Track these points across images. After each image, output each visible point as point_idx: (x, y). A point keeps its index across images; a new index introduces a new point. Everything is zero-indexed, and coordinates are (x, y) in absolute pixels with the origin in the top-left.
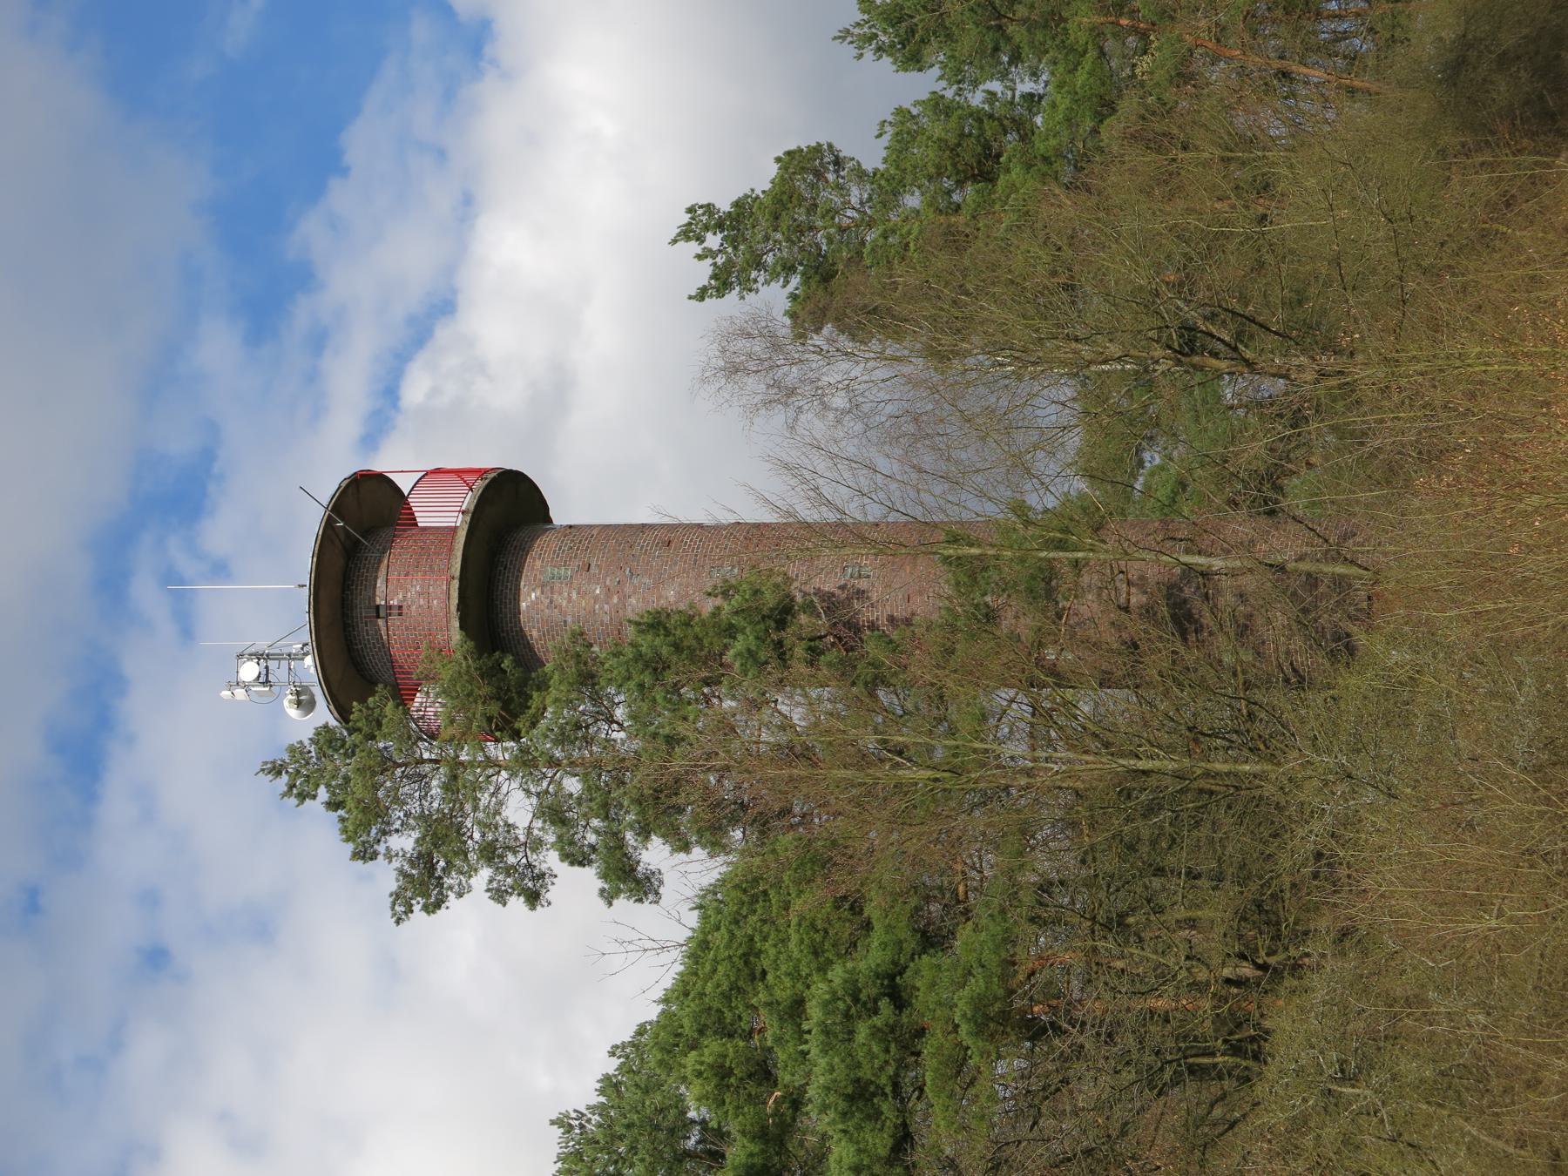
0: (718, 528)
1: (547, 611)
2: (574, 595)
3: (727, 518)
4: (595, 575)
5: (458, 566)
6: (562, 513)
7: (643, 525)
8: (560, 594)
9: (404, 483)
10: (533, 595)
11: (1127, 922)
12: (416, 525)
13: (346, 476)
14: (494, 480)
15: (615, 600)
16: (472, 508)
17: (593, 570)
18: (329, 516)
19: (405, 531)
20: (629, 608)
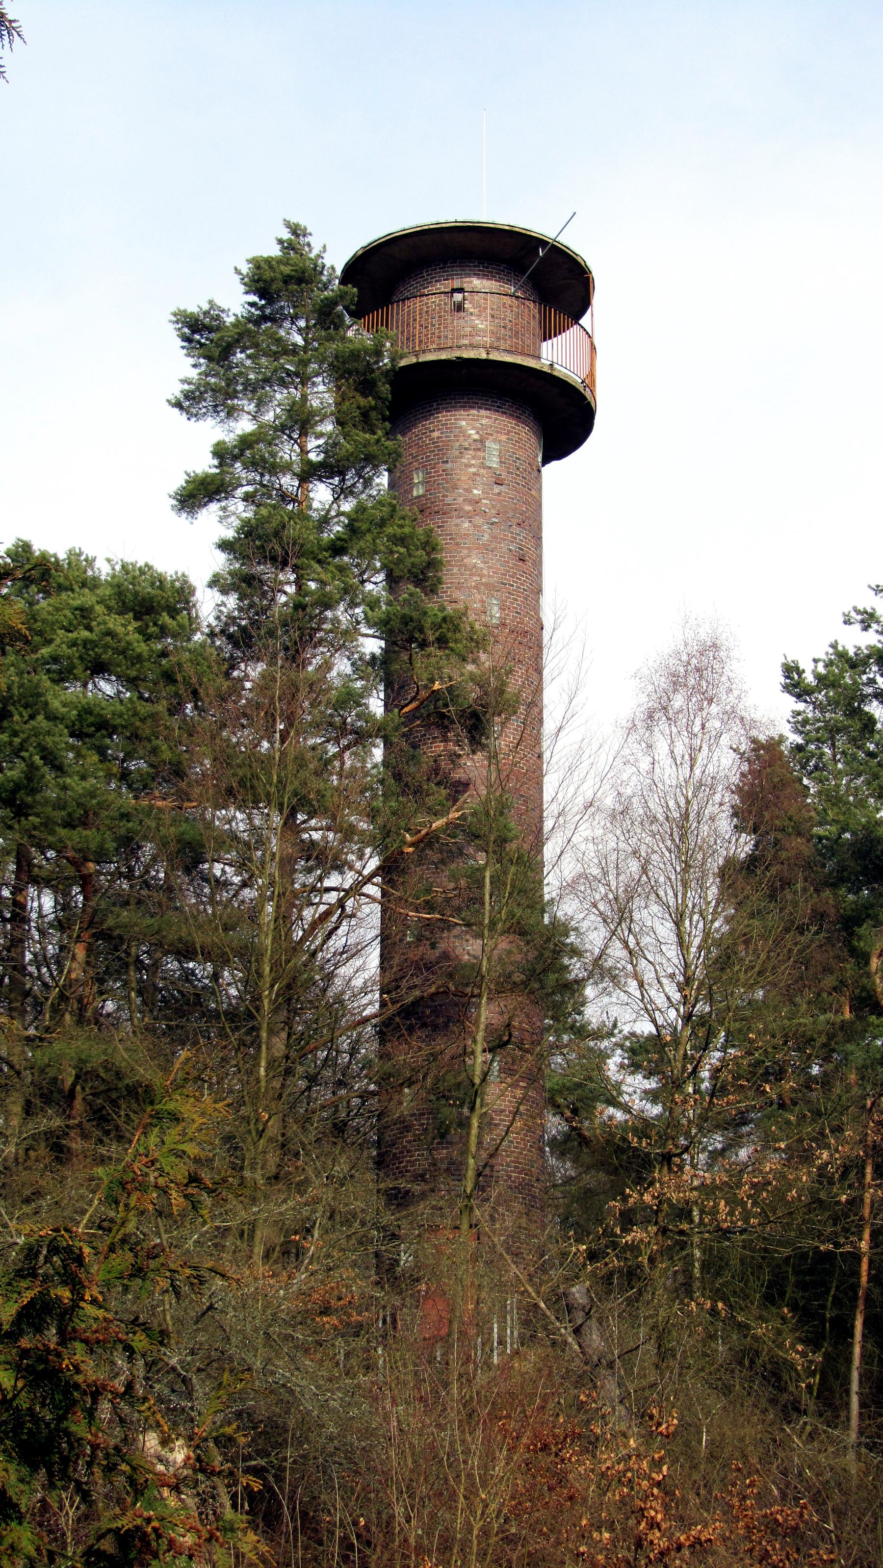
0: (536, 608)
1: (458, 444)
2: (473, 470)
3: (547, 617)
4: (492, 489)
5: (499, 358)
6: (553, 471)
7: (540, 538)
8: (474, 458)
9: (585, 321)
10: (473, 432)
11: (602, 1175)
12: (545, 340)
13: (588, 264)
14: (585, 398)
15: (468, 508)
16: (555, 373)
17: (497, 489)
18: (548, 243)
19: (540, 313)
20: (459, 521)
